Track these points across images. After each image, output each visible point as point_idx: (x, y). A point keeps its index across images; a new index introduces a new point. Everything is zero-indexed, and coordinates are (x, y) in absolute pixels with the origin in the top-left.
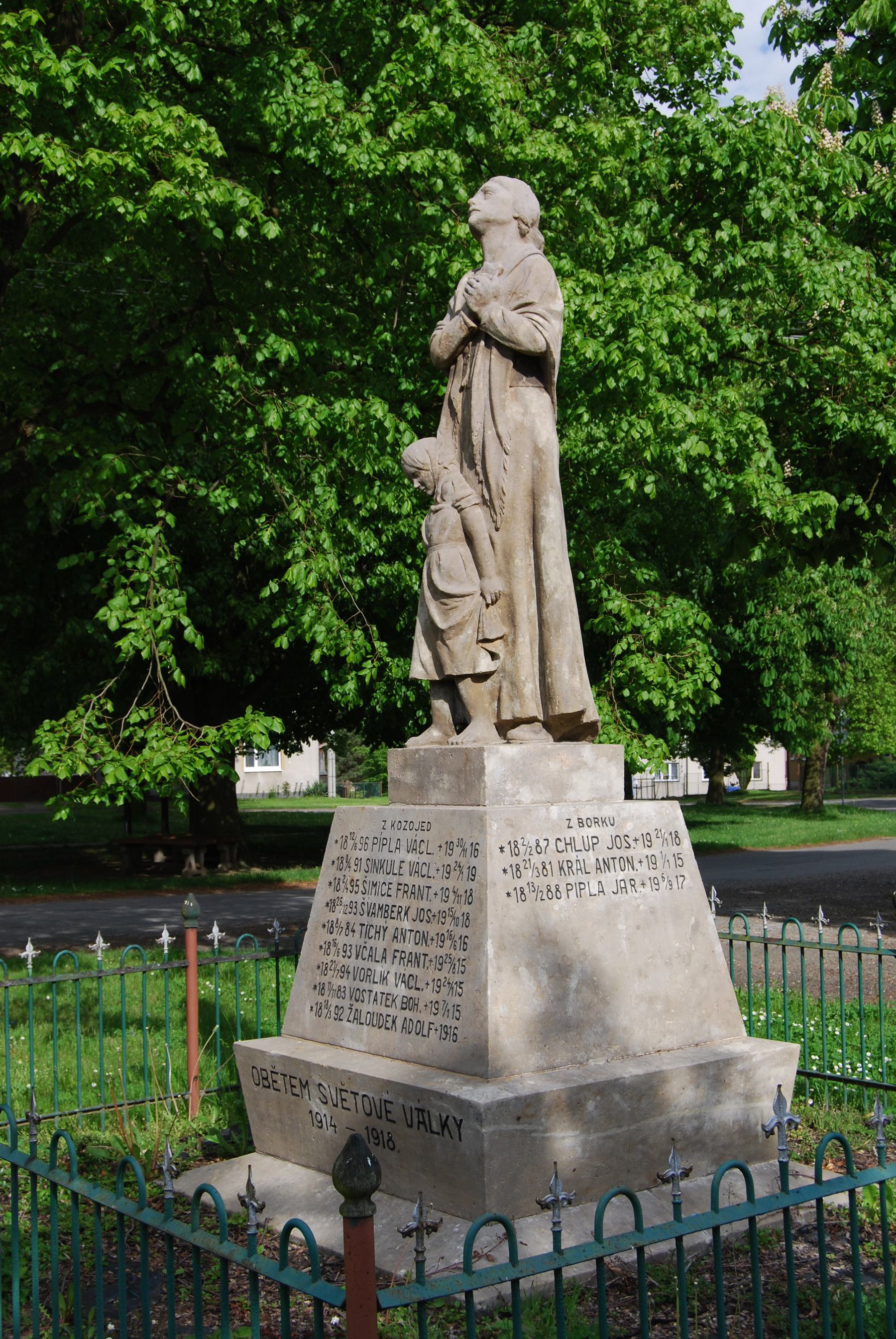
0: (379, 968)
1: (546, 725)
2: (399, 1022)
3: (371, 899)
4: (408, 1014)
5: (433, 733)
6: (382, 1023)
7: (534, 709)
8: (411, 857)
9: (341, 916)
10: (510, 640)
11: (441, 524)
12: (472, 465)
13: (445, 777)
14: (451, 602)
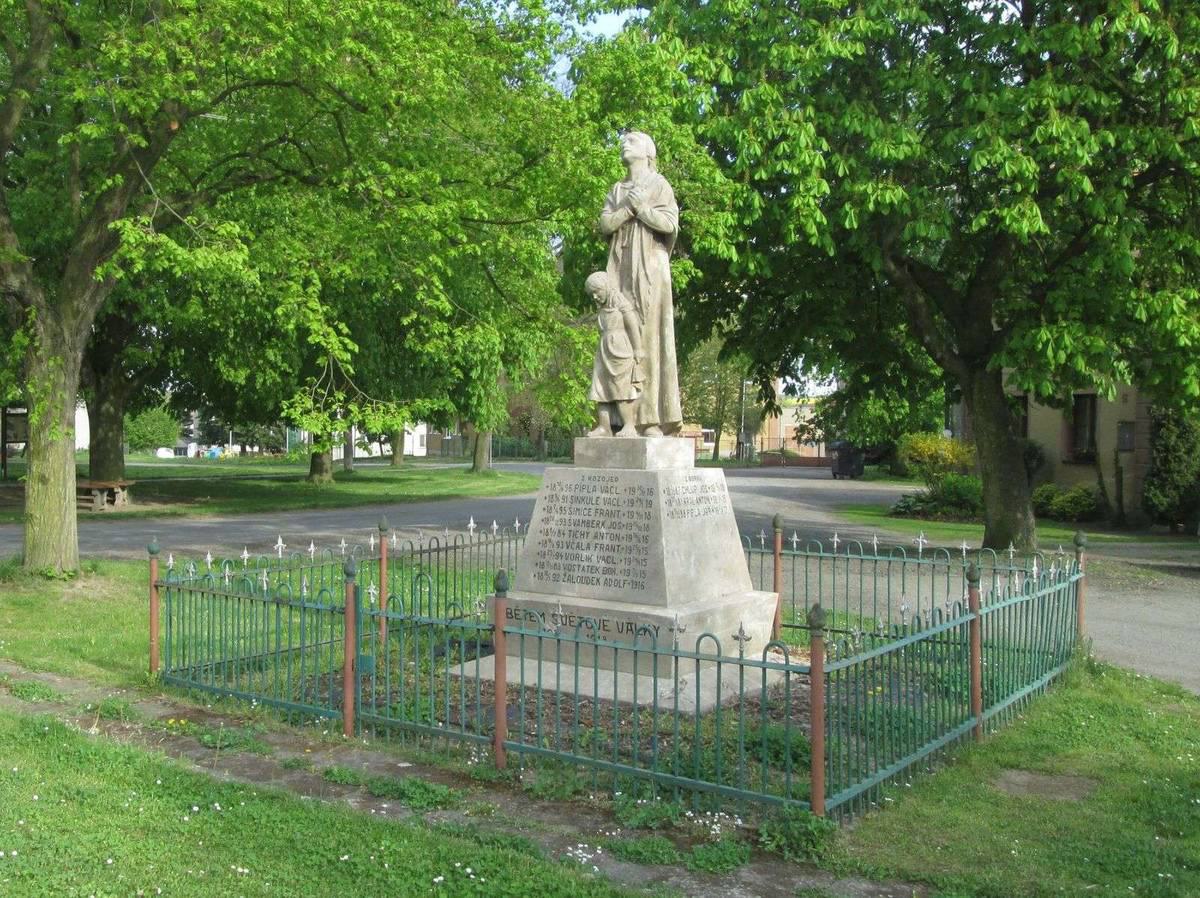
0: (585, 553)
1: (660, 427)
2: (602, 581)
3: (575, 517)
4: (608, 576)
5: (601, 430)
6: (587, 581)
7: (657, 420)
8: (604, 495)
9: (554, 527)
10: (648, 384)
11: (614, 318)
12: (630, 288)
13: (618, 454)
14: (620, 362)
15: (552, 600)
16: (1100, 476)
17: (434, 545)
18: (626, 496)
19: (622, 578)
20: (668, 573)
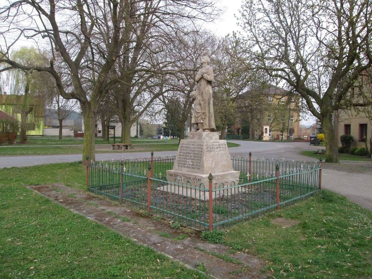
0: (188, 161)
6: (188, 167)
15: (180, 172)
16: (366, 145)
17: (167, 158)
18: (197, 147)
19: (195, 167)
20: (205, 166)
